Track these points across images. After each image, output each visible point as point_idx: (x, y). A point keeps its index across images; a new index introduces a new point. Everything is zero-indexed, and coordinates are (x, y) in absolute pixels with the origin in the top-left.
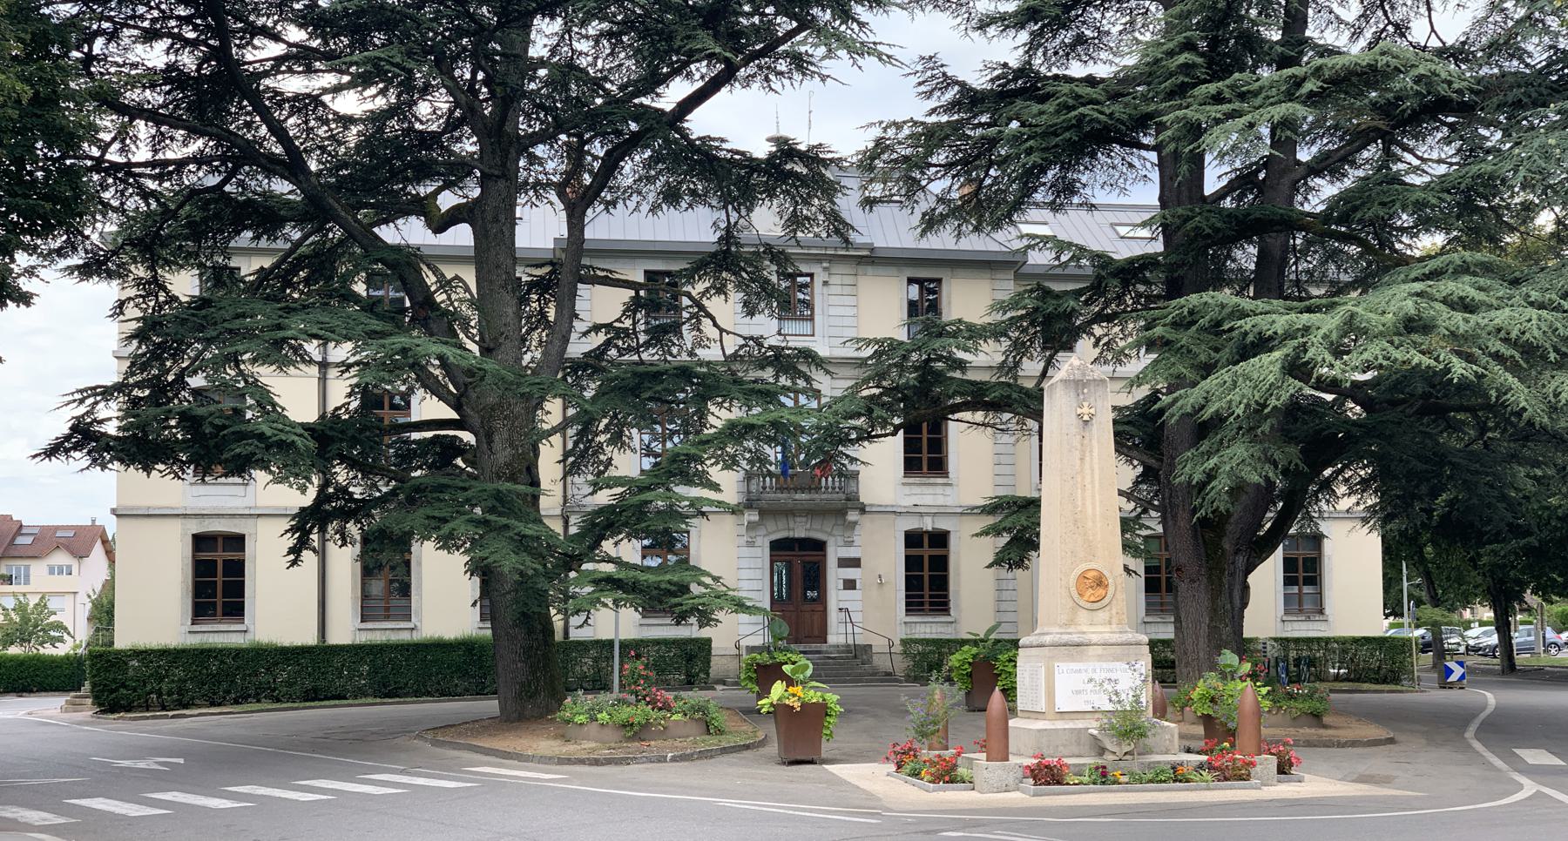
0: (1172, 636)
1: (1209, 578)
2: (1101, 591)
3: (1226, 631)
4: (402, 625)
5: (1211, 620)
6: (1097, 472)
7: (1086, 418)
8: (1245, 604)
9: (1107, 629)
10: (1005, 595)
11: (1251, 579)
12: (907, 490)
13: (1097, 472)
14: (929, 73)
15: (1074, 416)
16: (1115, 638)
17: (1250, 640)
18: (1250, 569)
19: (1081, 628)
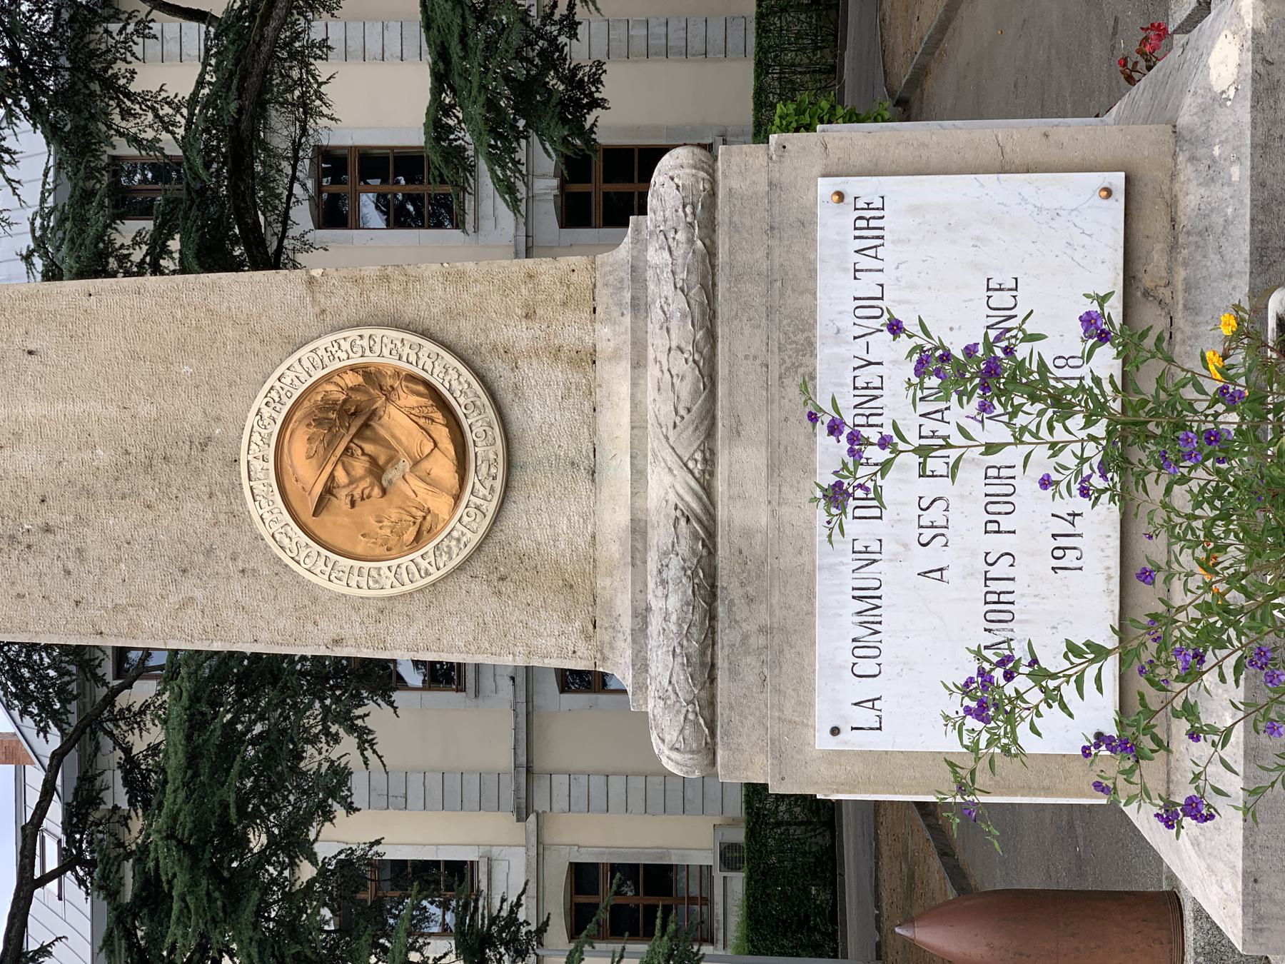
2: (399, 420)
9: (616, 380)
10: (676, 40)
12: (487, 224)
16: (670, 337)
19: (614, 548)
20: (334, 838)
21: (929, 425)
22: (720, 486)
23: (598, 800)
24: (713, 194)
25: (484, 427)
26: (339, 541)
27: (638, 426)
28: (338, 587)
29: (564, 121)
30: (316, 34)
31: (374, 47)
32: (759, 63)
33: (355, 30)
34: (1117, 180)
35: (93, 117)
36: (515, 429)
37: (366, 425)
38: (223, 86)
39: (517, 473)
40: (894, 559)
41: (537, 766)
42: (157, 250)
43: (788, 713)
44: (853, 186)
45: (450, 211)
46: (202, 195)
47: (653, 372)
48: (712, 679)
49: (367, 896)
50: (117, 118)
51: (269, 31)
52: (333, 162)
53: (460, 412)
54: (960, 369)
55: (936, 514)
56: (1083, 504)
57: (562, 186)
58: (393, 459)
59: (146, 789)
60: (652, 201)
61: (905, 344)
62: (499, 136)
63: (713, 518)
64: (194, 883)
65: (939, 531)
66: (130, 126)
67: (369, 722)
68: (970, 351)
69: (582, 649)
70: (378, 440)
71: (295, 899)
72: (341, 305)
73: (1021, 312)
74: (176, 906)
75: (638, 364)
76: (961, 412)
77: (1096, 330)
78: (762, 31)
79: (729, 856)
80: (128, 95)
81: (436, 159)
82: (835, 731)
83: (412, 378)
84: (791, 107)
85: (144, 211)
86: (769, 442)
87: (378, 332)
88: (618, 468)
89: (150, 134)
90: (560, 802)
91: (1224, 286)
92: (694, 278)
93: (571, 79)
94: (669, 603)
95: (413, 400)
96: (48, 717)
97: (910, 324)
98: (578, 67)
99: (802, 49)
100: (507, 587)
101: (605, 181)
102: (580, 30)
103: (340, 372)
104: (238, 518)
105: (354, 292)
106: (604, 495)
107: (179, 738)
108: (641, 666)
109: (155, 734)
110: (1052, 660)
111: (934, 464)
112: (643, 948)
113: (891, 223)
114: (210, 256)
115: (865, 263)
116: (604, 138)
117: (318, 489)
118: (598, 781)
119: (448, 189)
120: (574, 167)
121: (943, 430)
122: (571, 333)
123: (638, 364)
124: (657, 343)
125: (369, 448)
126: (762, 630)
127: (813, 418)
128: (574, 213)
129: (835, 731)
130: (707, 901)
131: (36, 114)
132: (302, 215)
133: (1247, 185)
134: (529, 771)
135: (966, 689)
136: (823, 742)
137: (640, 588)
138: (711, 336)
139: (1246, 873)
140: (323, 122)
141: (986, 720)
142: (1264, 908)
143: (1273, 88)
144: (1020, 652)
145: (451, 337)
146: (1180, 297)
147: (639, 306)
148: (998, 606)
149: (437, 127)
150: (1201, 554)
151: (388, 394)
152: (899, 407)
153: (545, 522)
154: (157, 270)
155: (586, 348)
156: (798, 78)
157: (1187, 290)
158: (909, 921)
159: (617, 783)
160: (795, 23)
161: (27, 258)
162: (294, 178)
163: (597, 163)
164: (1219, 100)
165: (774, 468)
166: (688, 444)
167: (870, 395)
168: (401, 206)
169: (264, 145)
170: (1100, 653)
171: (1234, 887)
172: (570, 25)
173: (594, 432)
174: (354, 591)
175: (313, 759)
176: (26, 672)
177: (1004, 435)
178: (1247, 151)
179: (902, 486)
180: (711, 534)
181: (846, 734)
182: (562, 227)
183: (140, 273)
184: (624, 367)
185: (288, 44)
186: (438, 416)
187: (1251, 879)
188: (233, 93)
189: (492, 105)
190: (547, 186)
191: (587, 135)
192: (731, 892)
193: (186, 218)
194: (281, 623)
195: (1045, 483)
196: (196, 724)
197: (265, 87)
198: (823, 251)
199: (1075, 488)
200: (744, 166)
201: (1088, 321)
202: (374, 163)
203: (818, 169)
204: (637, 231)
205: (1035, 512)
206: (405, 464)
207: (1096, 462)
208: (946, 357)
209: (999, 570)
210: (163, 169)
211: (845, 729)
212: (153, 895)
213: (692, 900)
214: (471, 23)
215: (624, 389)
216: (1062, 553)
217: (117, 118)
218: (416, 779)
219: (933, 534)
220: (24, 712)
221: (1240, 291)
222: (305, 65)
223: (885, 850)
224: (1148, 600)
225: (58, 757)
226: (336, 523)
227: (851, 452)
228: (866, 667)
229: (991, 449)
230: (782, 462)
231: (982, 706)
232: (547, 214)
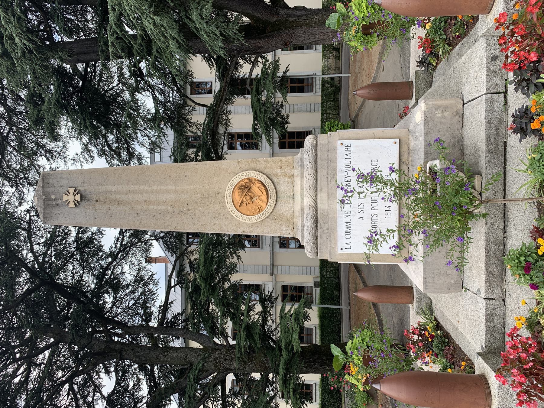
0: (321, 45)
1: (290, 28)
2: (256, 188)
3: (317, 18)
4: (314, 331)
5: (311, 26)
6: (132, 187)
7: (78, 198)
8: (304, 8)
9: (298, 180)
10: (304, 108)
11: (291, 5)
12: (264, 149)
13: (132, 187)
14: (82, 160)
15: (78, 210)
17: (323, 5)
18: (286, 6)
19: (297, 213)
20: (234, 278)
21: (360, 189)
22: (318, 201)
23: (288, 272)
24: (317, 144)
25: (271, 190)
26: (244, 212)
27: (302, 189)
28: (244, 221)
29: (281, 127)
30: (229, 109)
31: (240, 111)
32: (322, 113)
33: (236, 108)
34: (397, 140)
35: (183, 127)
36: (278, 190)
37: (249, 190)
38: (210, 120)
39: (278, 199)
40: (353, 215)
41: (275, 264)
42: (197, 155)
43: (332, 245)
44: (344, 142)
45: (256, 146)
46: (206, 144)
47: (305, 179)
48: (317, 239)
49: (239, 292)
50: (188, 128)
51: (219, 109)
52: (232, 136)
53: (267, 187)
54: (366, 177)
55: (361, 206)
56: (390, 204)
57: (280, 140)
58: (254, 196)
59: (194, 268)
60: (305, 145)
61: (355, 173)
62: (267, 130)
63: (317, 207)
64: (206, 286)
65: (362, 210)
66: (191, 129)
67: (240, 254)
68: (368, 174)
69: (291, 233)
70: (251, 192)
71: (224, 291)
72: (237, 165)
73: (378, 166)
74: (202, 291)
75: (302, 177)
76: (366, 185)
77: (392, 170)
78: (323, 106)
79: (316, 284)
80: (191, 123)
81: (254, 135)
82: (342, 249)
83: (258, 180)
84: (329, 123)
85: (193, 147)
86: (328, 192)
87: (251, 172)
88: (298, 197)
89: (195, 131)
90: (280, 272)
91: (419, 161)
92: (313, 161)
93: (282, 118)
94: (308, 224)
95: (258, 185)
96: (173, 252)
97: (356, 169)
98: (284, 115)
99: (331, 110)
100: (276, 221)
101: (289, 139)
102: (284, 107)
103: (244, 179)
104: (224, 207)
105: (247, 164)
106: (295, 203)
107: (202, 256)
108: (303, 236)
109: (196, 256)
110: (384, 232)
111: (361, 196)
112: (298, 304)
113: (352, 149)
114: (208, 157)
115: (347, 157)
116: (289, 130)
117: (240, 202)
118: (288, 267)
119: (256, 141)
120: (282, 136)
121: (362, 189)
122: (289, 171)
123: (302, 177)
124: (306, 173)
125: (250, 194)
126: (327, 229)
127: (338, 187)
128: (282, 146)
129: (342, 249)
130: (311, 294)
131: (172, 127)
132: (225, 147)
133: (423, 141)
134: (273, 265)
135: (368, 238)
136: (339, 251)
137: (303, 221)
138: (316, 172)
139: (424, 277)
140: (230, 127)
141: (372, 243)
142: (428, 284)
143: (428, 122)
144: (378, 230)
145: (265, 172)
146: (410, 163)
147: (302, 166)
148: (374, 224)
149: (254, 129)
150: (412, 212)
151: (253, 183)
152: (354, 184)
153: (284, 208)
154: (197, 160)
155: (291, 174)
156: (330, 116)
157: (412, 162)
158: (356, 291)
159: (292, 268)
160: (330, 104)
161: (170, 157)
162: (225, 140)
163: (287, 135)
164: (418, 124)
165: (329, 197)
166: (312, 193)
167: (348, 183)
168: (245, 145)
169: (218, 133)
170: (393, 231)
171: (421, 280)
172: (282, 106)
173: (293, 191)
174: (247, 222)
175: (228, 262)
176: (169, 243)
177: (375, 190)
178: (423, 134)
179: (355, 200)
180: (317, 210)
181: (344, 250)
182: (280, 148)
183: (193, 161)
184: (299, 178)
185: (223, 112)
186: (263, 188)
187: (425, 278)
188: (212, 122)
189: (266, 124)
190: (276, 140)
191: (285, 129)
192: (317, 292)
193: (203, 148)
194: (233, 228)
195: (383, 199)
196: (206, 253)
197: (218, 120)
198: (338, 155)
199: (389, 200)
200: (323, 138)
201: (390, 168)
202: (240, 136)
203: (338, 139)
204: (302, 151)
205: (382, 205)
206: (257, 197)
207: (392, 195)
208: (363, 175)
209: (375, 217)
210: (196, 138)
211: (344, 249)
212: (197, 289)
213: (308, 294)
214: (261, 106)
215: (299, 182)
216: (387, 214)
217: (188, 128)
218: (249, 267)
219: (361, 210)
220: (168, 252)
221: (422, 162)
222: (226, 116)
223: (351, 283)
224: (403, 222)
225: (176, 261)
226: (244, 208)
227: (345, 193)
228: (348, 236)
229: (372, 193)
230: (331, 196)
231: (371, 241)
232: (276, 146)
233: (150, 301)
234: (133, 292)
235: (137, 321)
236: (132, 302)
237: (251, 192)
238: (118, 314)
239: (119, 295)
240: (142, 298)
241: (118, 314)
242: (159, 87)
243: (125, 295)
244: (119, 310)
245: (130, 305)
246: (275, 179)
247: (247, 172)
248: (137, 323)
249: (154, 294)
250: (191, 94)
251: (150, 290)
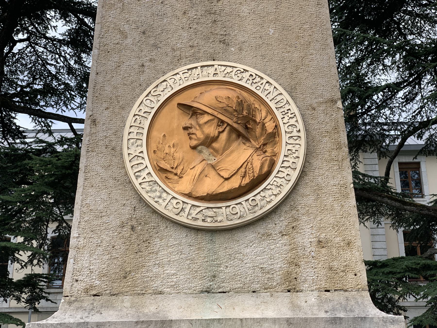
2: (241, 156)
28: (130, 120)
31: (377, 245)
36: (239, 235)
39: (208, 237)
53: (250, 196)
83: (272, 164)
87: (303, 142)
95: (257, 163)
100: (126, 232)
103: (274, 118)
104: (178, 61)
105: (329, 127)
106: (191, 300)
122: (311, 274)
125: (224, 136)
145: (302, 190)
151: (261, 149)
173: (238, 291)
174: (127, 130)
186: (247, 180)
226: (175, 119)
233: (54, 98)
234: (70, 71)
235: (21, 77)
236: (53, 70)
237: (229, 141)
238: (33, 48)
239: (66, 48)
240: (60, 85)
241: (33, 48)
242: (416, 94)
243: (65, 57)
244: (41, 49)
245: (48, 67)
246: (281, 223)
247: (300, 126)
248: (18, 79)
249: (66, 106)
250: (400, 164)
251: (72, 98)
